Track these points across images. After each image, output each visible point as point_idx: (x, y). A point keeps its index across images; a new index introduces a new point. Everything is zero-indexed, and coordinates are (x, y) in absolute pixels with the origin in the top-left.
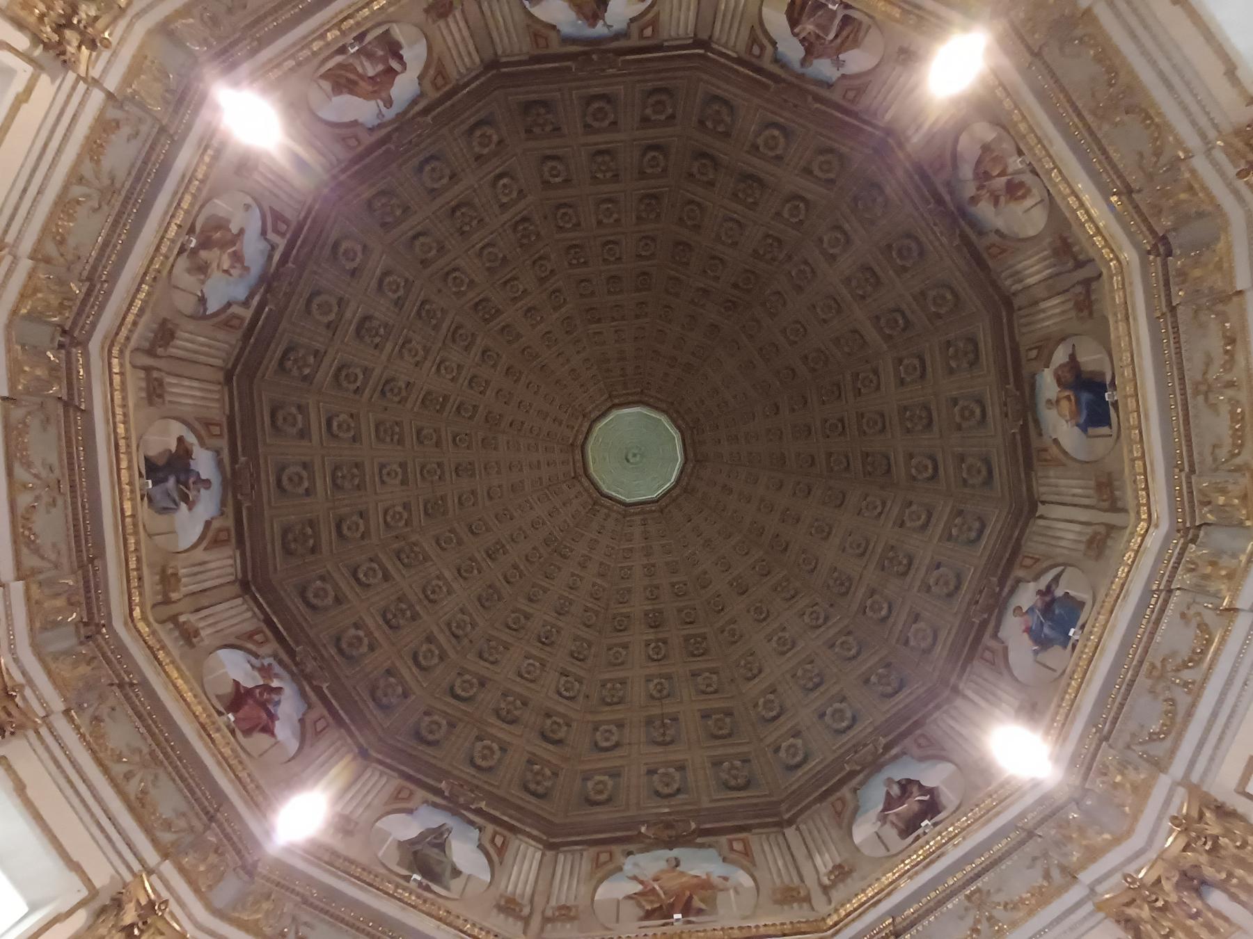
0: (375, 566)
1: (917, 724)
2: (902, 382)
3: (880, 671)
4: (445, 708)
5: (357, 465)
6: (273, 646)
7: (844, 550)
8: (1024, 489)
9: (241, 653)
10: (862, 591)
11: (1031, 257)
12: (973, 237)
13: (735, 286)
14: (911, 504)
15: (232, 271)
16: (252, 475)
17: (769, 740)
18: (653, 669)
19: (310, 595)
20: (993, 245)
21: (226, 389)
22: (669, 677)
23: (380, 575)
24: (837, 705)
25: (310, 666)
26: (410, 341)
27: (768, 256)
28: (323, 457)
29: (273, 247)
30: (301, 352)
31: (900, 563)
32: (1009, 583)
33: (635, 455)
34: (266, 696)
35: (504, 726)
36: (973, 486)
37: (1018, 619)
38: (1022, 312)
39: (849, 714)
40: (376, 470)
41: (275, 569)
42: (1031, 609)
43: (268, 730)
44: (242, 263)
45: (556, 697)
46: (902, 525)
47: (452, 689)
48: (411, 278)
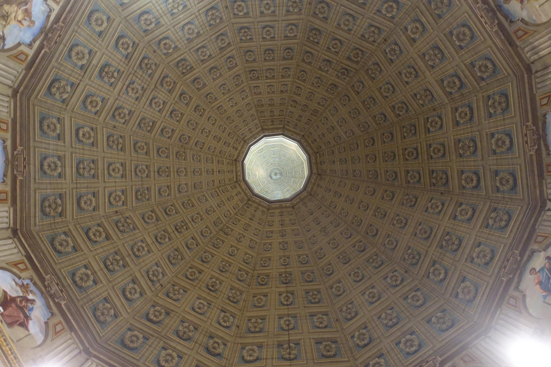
0: (100, 229)
1: (463, 348)
2: (458, 124)
3: (439, 314)
4: (141, 327)
5: (93, 162)
6: (30, 273)
7: (415, 235)
8: (538, 192)
9: (9, 274)
10: (428, 260)
11: (544, 36)
12: (506, 24)
13: (349, 58)
14: (461, 204)
15: (23, 22)
16: (25, 159)
17: (360, 360)
18: (284, 311)
19: (57, 244)
20: (520, 29)
21: (12, 101)
22: (295, 317)
23: (104, 235)
24: (408, 337)
25: (55, 288)
26: (133, 83)
27: (371, 39)
28: (72, 154)
29: (51, 11)
30: (63, 83)
31: (453, 244)
32: (527, 253)
33: (276, 174)
34: (24, 303)
35: (182, 342)
36: (503, 192)
37: (532, 277)
38: (538, 74)
39: (416, 343)
40: (106, 166)
41: (35, 224)
42: (542, 269)
43: (24, 325)
44: (30, 18)
45: (217, 326)
46: (455, 218)
47: (147, 314)
48: (137, 41)
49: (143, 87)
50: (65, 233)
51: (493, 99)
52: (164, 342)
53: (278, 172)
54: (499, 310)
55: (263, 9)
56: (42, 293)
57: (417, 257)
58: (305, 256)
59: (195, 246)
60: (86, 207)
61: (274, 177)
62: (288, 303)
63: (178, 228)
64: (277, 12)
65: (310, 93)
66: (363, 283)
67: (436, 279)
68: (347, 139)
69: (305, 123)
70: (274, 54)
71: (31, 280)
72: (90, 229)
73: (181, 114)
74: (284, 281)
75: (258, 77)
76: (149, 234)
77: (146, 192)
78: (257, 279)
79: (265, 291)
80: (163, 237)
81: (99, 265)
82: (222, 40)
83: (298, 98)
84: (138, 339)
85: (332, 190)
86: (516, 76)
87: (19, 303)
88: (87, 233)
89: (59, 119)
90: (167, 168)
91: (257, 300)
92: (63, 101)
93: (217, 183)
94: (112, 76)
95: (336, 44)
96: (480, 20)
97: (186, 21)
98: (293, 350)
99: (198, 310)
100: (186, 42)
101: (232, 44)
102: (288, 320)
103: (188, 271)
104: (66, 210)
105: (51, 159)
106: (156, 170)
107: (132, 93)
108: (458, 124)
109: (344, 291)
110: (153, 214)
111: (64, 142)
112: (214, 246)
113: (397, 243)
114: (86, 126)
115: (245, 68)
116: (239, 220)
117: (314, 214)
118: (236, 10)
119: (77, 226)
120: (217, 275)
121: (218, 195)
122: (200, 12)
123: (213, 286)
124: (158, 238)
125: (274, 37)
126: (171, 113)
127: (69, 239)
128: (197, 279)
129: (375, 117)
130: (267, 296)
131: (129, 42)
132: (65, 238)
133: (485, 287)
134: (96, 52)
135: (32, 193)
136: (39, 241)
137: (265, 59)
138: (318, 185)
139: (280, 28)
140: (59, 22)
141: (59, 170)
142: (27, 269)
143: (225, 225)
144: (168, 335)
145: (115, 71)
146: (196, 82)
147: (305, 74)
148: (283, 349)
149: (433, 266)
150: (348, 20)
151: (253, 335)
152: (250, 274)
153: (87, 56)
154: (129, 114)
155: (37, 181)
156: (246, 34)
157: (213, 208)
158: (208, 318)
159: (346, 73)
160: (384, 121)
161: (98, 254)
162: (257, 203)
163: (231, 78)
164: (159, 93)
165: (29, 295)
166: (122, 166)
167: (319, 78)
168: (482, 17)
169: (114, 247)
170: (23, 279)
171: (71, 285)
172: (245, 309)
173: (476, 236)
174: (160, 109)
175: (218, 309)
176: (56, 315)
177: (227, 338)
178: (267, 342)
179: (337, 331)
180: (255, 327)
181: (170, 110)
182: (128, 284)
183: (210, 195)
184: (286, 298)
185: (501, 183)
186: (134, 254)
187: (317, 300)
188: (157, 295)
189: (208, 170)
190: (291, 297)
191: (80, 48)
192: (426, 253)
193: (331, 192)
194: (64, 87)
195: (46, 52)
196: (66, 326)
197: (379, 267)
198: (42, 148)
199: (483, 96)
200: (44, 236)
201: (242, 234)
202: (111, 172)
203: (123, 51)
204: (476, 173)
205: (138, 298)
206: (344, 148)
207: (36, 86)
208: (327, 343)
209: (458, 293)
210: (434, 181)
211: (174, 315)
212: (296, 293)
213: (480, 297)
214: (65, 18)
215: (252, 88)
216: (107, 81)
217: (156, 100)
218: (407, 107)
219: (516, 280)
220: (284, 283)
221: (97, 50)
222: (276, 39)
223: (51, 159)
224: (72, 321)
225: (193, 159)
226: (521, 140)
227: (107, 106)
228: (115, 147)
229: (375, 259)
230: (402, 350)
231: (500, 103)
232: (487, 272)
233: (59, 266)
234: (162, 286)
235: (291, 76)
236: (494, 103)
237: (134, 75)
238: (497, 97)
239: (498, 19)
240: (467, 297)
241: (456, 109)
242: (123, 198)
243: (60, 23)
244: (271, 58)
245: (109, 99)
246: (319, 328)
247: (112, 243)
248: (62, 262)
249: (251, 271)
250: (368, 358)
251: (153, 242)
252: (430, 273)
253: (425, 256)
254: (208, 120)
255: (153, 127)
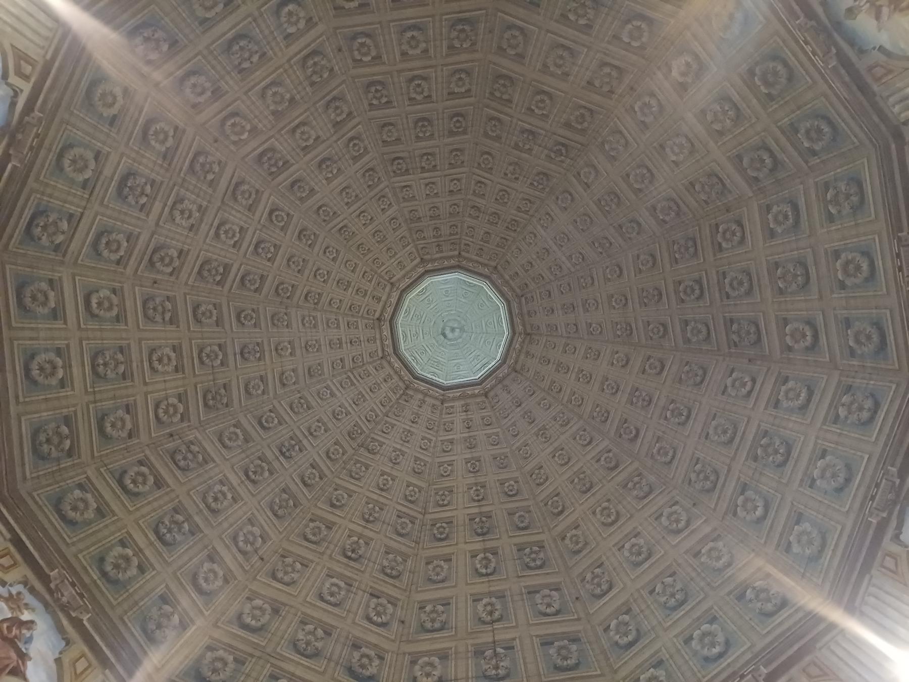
2: (772, 234)
5: (121, 350)
6: (23, 570)
10: (731, 486)
13: (568, 125)
14: (786, 380)
17: (623, 673)
22: (501, 596)
23: (151, 480)
24: (706, 627)
25: (68, 594)
26: (182, 201)
29: (16, 93)
34: (15, 631)
35: (304, 661)
39: (721, 638)
41: (25, 478)
46: (777, 405)
47: (240, 616)
49: (201, 206)
50: (80, 486)
51: (835, 188)
52: (273, 665)
53: (456, 325)
54: (867, 577)
55: (405, 47)
56: (46, 605)
57: (712, 478)
58: (512, 483)
59: (317, 479)
60: (114, 434)
61: (450, 335)
62: (489, 571)
63: (284, 450)
64: (432, 51)
65: (501, 191)
66: (619, 528)
67: (748, 518)
68: (573, 270)
69: (498, 246)
70: (432, 126)
71: (25, 583)
72: (125, 472)
73: (275, 246)
74: (479, 531)
75: (407, 170)
76: (232, 468)
77: (223, 391)
78: (431, 530)
79: (447, 550)
80: (258, 471)
81: (146, 536)
82: (337, 108)
83: (480, 201)
84: (226, 664)
85: (552, 361)
86: (874, 146)
87: (5, 632)
88: (120, 482)
89: (51, 282)
90: (258, 344)
91: (434, 569)
92: (57, 248)
93: (348, 364)
94: (142, 193)
95: (542, 101)
96: (802, 48)
97: (268, 81)
98: (502, 661)
99: (329, 598)
100: (271, 118)
101: (355, 114)
102: (491, 604)
103: (307, 526)
104: (78, 442)
105: (43, 356)
106: (238, 350)
107: (182, 218)
108: (772, 234)
109: (586, 544)
110: (238, 431)
111: (65, 323)
112: (351, 477)
113: (675, 452)
114: (102, 288)
115: (383, 154)
116: (393, 426)
117: (523, 405)
118: (356, 53)
119: (102, 470)
120: (359, 529)
121: (353, 384)
122: (292, 62)
123: (353, 551)
124: (251, 473)
125: (430, 96)
126: (257, 246)
127: (89, 496)
128: (323, 540)
129: (620, 226)
130: (451, 560)
131: (166, 129)
132: (81, 495)
133: (838, 532)
134: (109, 153)
135: (14, 423)
136: (34, 507)
137: (417, 137)
138: (527, 353)
139: (440, 80)
140: (32, 110)
141: (60, 373)
142: (15, 564)
143: (368, 437)
144: (278, 650)
145: (146, 184)
146: (296, 187)
147: (490, 158)
148: (485, 658)
149: (742, 493)
150: (561, 57)
151: (429, 636)
152: (417, 522)
153: (92, 165)
154: (179, 257)
155: (21, 399)
156: (378, 95)
157: (346, 408)
158: (349, 611)
159: (564, 151)
160: (638, 234)
161: (143, 516)
162: (421, 392)
163: (358, 175)
164: (230, 214)
165: (23, 614)
166: (175, 352)
167: (517, 164)
168: (806, 43)
169: (173, 500)
170: (11, 585)
171: (98, 581)
172: (414, 587)
173: (817, 438)
174: (236, 242)
175: (364, 591)
176: (74, 643)
177: (385, 645)
178: (456, 647)
179: (579, 619)
180: (433, 621)
181: (254, 241)
182: (202, 563)
183: (338, 386)
184: (484, 562)
185: (858, 341)
186: (208, 507)
187: (538, 563)
188: (255, 579)
189: (330, 341)
190: (493, 560)
191: (77, 151)
192: (729, 471)
193: (550, 365)
194: (55, 223)
195: (14, 167)
196: (94, 662)
197: (645, 497)
198: (24, 339)
199: (816, 183)
200: (42, 496)
201: (400, 450)
202: (156, 364)
203: (157, 146)
204: (810, 323)
205: (222, 587)
206: (569, 285)
207: (15, 205)
208: (561, 643)
209: (789, 544)
210: (735, 337)
211: (288, 612)
212: (500, 552)
213: (830, 553)
214: (45, 102)
215: (398, 190)
216: (133, 203)
217: (227, 227)
218: (678, 206)
219: (894, 523)
220: (479, 535)
221: (109, 150)
222: (434, 98)
223: (43, 356)
224: (104, 648)
225: (304, 325)
226: (889, 264)
227: (138, 247)
228: (158, 318)
229: (637, 483)
230: (695, 653)
231: (848, 196)
232: (841, 506)
233: (74, 549)
234: (262, 559)
235: (465, 164)
236: (836, 195)
237: (182, 186)
238: (842, 187)
239: (836, 45)
240: (808, 552)
241: (769, 208)
242: (181, 408)
243: (37, 114)
244: (428, 134)
245: (140, 233)
246: (546, 615)
247: (167, 494)
248: (80, 540)
249: (420, 516)
250: (638, 667)
251: (242, 482)
252: (737, 506)
253: (727, 476)
254: (325, 252)
255: (225, 275)
